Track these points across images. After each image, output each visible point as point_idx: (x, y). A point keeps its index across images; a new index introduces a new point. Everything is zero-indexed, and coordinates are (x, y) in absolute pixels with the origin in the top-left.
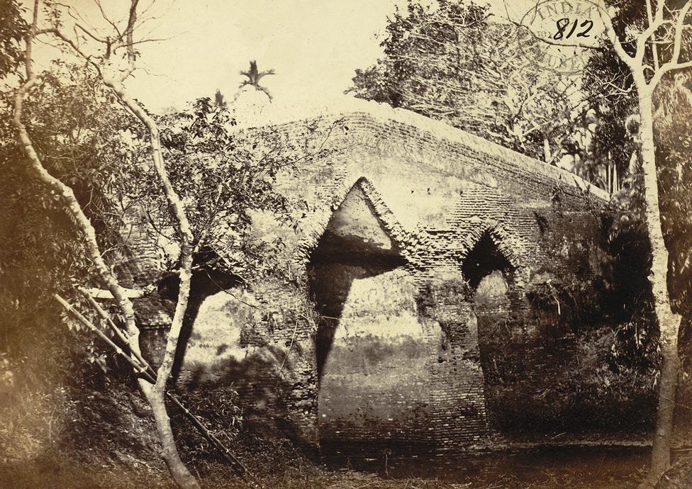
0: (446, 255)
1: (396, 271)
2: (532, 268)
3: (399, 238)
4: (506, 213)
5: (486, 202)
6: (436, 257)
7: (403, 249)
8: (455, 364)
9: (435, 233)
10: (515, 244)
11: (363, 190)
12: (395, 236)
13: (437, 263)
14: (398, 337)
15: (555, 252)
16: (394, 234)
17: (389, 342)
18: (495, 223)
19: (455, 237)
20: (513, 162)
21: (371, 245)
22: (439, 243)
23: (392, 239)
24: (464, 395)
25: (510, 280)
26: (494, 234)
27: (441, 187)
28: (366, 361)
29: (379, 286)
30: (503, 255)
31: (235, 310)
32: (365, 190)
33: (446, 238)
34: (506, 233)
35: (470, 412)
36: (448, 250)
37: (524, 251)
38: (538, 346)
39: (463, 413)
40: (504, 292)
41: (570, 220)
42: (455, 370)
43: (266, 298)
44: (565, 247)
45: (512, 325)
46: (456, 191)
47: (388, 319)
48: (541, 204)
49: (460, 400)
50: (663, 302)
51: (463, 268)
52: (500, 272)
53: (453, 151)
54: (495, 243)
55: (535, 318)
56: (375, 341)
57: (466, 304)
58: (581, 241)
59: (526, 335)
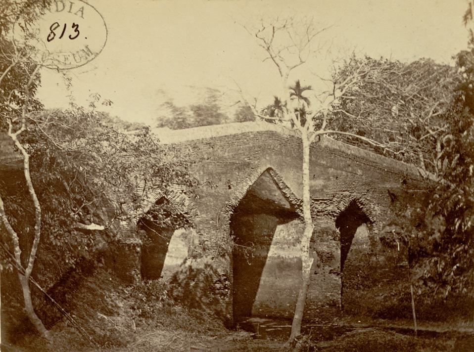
0: (325, 213)
1: (294, 221)
2: (384, 222)
3: (294, 202)
4: (368, 190)
5: (354, 183)
6: (318, 214)
7: (297, 208)
8: (324, 276)
9: (318, 200)
10: (375, 209)
11: (271, 174)
12: (291, 201)
13: (318, 217)
14: (293, 258)
15: (401, 214)
16: (291, 199)
17: (289, 261)
18: (359, 196)
19: (331, 203)
20: (374, 160)
21: (280, 206)
22: (321, 206)
23: (290, 202)
24: (329, 294)
25: (370, 229)
26: (360, 202)
27: (323, 174)
28: (277, 271)
29: (285, 229)
30: (365, 214)
31: (186, 238)
32: (272, 174)
33: (325, 203)
34: (367, 202)
35: (333, 304)
36: (326, 210)
37: (379, 212)
38: (385, 268)
39: (328, 304)
40: (367, 236)
41: (413, 195)
42: (324, 279)
43: (202, 232)
44: (408, 211)
45: (370, 255)
46: (333, 176)
47: (289, 247)
48: (395, 185)
49: (326, 297)
50: (305, 252)
51: (336, 221)
52: (365, 224)
53: (332, 153)
54: (361, 207)
55: (384, 251)
56: (282, 259)
57: (333, 242)
58: (420, 208)
59: (379, 261)
